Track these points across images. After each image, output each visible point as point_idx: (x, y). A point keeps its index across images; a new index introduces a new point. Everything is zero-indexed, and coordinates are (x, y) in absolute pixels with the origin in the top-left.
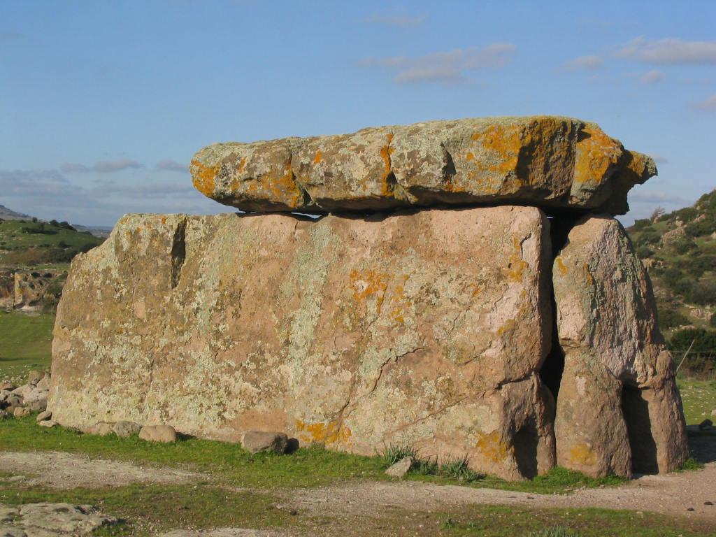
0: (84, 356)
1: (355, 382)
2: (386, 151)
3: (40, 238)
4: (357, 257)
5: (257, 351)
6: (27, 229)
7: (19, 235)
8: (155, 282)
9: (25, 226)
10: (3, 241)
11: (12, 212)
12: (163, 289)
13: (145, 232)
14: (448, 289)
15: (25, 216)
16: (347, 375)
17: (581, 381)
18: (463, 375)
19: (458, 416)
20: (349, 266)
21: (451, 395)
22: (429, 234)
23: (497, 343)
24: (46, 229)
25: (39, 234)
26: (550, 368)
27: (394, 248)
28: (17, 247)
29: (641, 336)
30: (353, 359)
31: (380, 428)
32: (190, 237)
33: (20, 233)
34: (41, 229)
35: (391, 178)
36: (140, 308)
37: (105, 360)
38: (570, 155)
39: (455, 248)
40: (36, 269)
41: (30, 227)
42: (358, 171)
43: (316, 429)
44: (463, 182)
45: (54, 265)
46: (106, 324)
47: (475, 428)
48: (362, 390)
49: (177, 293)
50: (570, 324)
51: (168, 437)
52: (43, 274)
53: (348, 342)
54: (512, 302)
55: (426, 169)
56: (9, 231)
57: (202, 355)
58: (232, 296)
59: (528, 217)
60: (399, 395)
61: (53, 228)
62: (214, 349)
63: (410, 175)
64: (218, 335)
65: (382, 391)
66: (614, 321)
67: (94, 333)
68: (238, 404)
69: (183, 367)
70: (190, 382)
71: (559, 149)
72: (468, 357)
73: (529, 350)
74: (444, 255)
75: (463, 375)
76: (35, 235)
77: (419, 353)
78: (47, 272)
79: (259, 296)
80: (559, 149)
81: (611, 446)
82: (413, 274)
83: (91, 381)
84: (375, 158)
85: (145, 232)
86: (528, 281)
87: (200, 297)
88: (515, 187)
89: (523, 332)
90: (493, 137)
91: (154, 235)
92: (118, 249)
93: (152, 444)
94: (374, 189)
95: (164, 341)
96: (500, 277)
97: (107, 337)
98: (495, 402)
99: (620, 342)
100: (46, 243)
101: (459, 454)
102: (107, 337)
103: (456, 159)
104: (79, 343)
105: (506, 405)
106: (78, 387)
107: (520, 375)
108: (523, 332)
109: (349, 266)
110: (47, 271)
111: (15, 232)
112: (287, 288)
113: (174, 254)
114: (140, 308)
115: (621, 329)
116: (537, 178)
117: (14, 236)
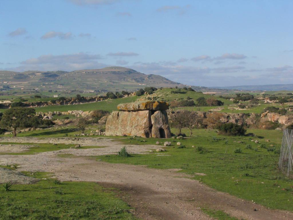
0: (109, 128)
1: (132, 129)
2: (134, 105)
3: (179, 96)
4: (134, 116)
5: (124, 126)
6: (173, 92)
7: (170, 95)
8: (116, 119)
9: (172, 90)
10: (162, 98)
11: (172, 82)
12: (116, 120)
13: (115, 113)
14: (140, 119)
15: (178, 84)
16: (131, 128)
17: (154, 128)
18: (141, 128)
19: (140, 132)
20: (132, 117)
21: (140, 130)
22: (139, 113)
23: (144, 124)
24: (182, 91)
25: (178, 94)
26: (151, 127)
27: (136, 115)
28: (169, 100)
29: (163, 123)
30: (132, 126)
31: (134, 133)
32: (119, 114)
33: (170, 94)
34: (179, 91)
35: (134, 108)
36: (114, 122)
37: (111, 128)
38: (153, 105)
39: (141, 115)
40: (174, 110)
41: (174, 91)
42: (131, 107)
43: (129, 134)
44: (141, 108)
45: (183, 108)
46: (111, 124)
47: (141, 133)
48: (133, 129)
49: (118, 120)
50: (153, 122)
51: (115, 136)
52: (176, 112)
53: (131, 125)
54: (146, 120)
55: (137, 107)
56: (165, 93)
57: (120, 127)
58: (123, 120)
59: (147, 111)
60: (136, 130)
61: (185, 91)
62: (121, 126)
63: (136, 108)
64: (121, 125)
65: (134, 130)
66: (159, 122)
67: (110, 125)
68: (123, 132)
69: (118, 128)
70: (119, 130)
71: (151, 104)
72: (141, 126)
73: (147, 124)
74: (140, 116)
75: (141, 128)
76: (176, 94)
77: (137, 126)
78: (178, 111)
79: (125, 120)
80: (151, 104)
81: (157, 135)
82: (138, 117)
83: (109, 130)
84: (133, 106)
85: (115, 113)
86: (147, 118)
87: (120, 121)
88: (145, 109)
89: (146, 123)
90: (143, 104)
91: (115, 114)
92: (112, 115)
93: (114, 136)
94: (133, 109)
95: (116, 126)
96: (144, 118)
97: (111, 125)
98: (143, 130)
99: (160, 124)
100: (182, 98)
101: (140, 135)
102: (111, 125)
103: (140, 106)
104: (108, 126)
105: (144, 130)
106: (108, 131)
107: (146, 127)
108: (146, 123)
109: (132, 117)
110: (178, 110)
111: (168, 93)
112: (127, 119)
113: (117, 116)
114: (114, 122)
115: (160, 123)
116: (148, 107)
117: (167, 95)
